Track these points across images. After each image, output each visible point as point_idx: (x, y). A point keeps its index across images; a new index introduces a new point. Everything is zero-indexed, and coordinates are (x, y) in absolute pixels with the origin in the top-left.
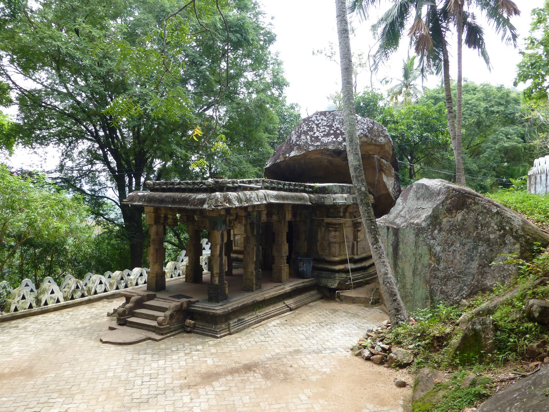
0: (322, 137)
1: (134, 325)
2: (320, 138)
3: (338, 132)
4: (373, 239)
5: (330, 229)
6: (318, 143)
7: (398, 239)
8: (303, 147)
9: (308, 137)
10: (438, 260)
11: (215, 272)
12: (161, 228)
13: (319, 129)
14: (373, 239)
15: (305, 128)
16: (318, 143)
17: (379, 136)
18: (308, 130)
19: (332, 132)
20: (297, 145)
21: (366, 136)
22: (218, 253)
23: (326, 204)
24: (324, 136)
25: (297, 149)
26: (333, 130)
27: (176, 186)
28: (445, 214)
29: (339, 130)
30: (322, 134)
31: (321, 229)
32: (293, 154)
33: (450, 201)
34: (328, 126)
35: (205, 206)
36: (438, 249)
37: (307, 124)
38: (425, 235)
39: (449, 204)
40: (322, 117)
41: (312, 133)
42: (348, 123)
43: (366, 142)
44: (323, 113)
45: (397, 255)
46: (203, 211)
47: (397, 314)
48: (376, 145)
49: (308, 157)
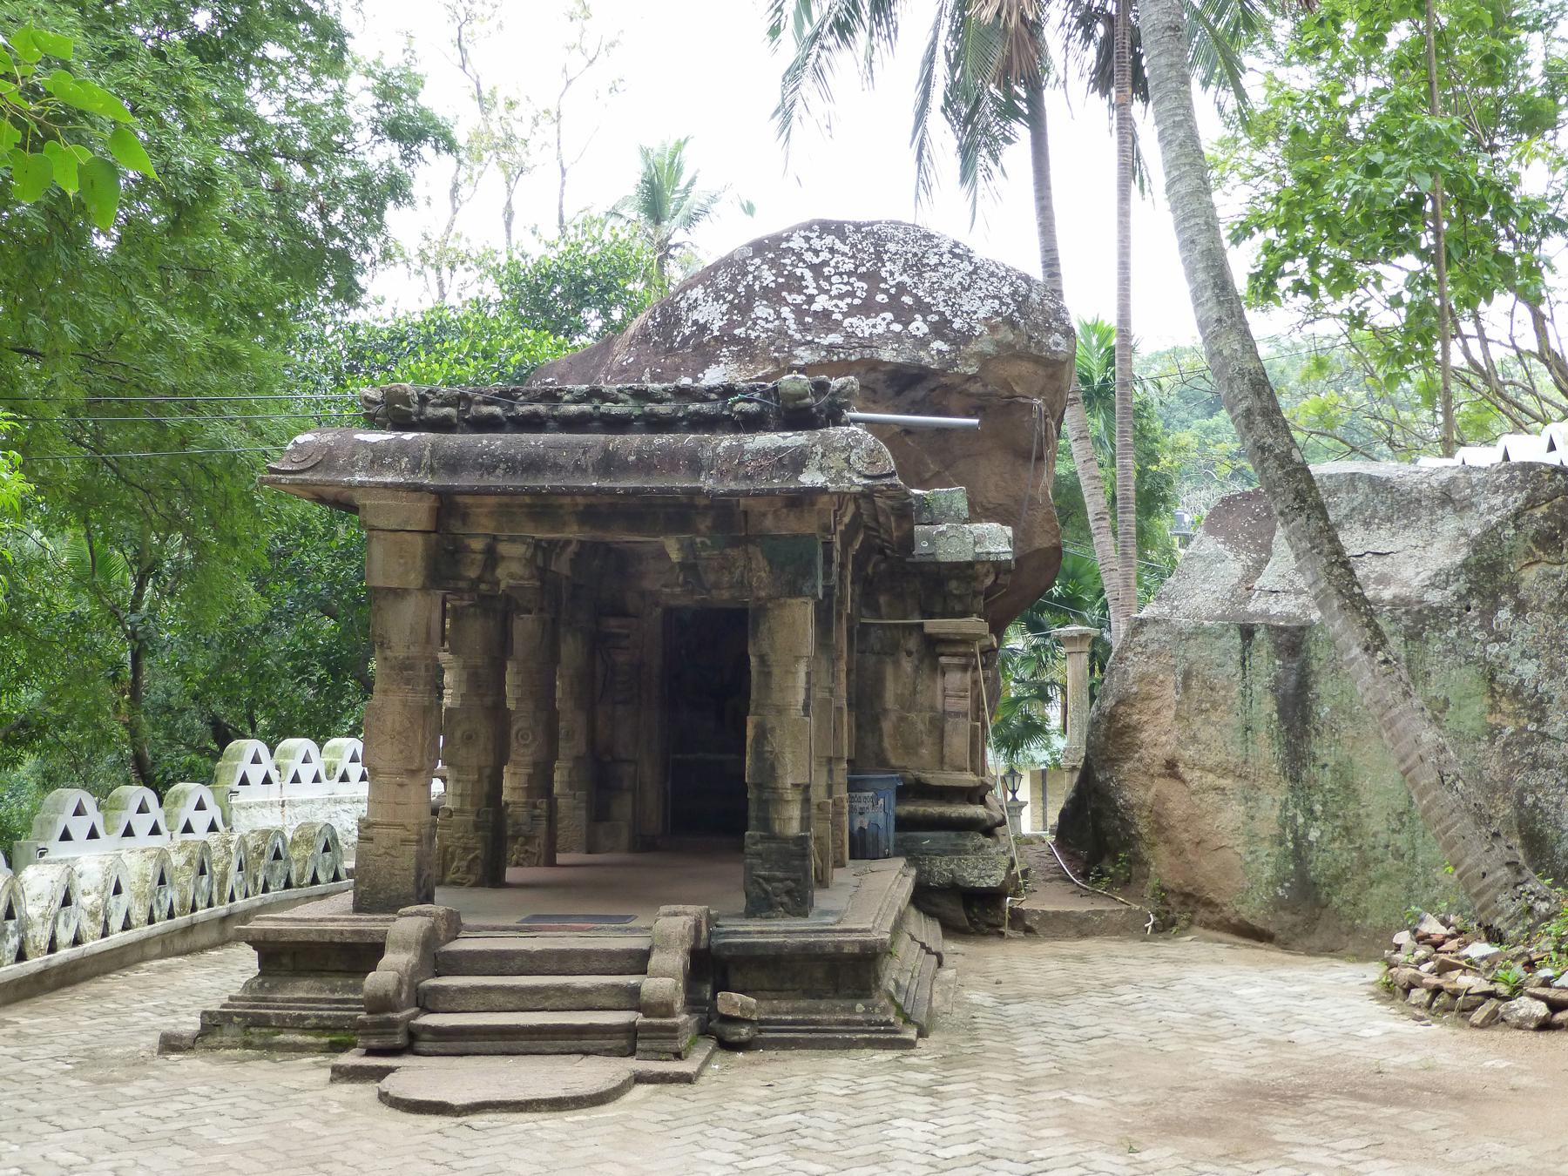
0: (845, 315)
1: (473, 1045)
4: (1368, 632)
5: (943, 660)
6: (835, 338)
7: (1305, 665)
8: (765, 350)
9: (786, 312)
10: (1538, 707)
11: (789, 781)
14: (1368, 632)
15: (768, 277)
16: (835, 338)
17: (1049, 329)
18: (780, 287)
19: (881, 298)
20: (735, 340)
22: (801, 697)
23: (942, 558)
24: (852, 311)
25: (737, 357)
26: (886, 291)
27: (573, 408)
28: (1529, 553)
31: (897, 664)
32: (713, 376)
33: (1544, 508)
34: (861, 277)
35: (811, 478)
36: (1529, 669)
37: (773, 264)
38: (1452, 633)
39: (1545, 518)
40: (829, 240)
41: (799, 299)
42: (1201, 221)
43: (1010, 346)
44: (836, 229)
45: (1305, 720)
46: (802, 499)
47: (1519, 879)
48: (1037, 360)
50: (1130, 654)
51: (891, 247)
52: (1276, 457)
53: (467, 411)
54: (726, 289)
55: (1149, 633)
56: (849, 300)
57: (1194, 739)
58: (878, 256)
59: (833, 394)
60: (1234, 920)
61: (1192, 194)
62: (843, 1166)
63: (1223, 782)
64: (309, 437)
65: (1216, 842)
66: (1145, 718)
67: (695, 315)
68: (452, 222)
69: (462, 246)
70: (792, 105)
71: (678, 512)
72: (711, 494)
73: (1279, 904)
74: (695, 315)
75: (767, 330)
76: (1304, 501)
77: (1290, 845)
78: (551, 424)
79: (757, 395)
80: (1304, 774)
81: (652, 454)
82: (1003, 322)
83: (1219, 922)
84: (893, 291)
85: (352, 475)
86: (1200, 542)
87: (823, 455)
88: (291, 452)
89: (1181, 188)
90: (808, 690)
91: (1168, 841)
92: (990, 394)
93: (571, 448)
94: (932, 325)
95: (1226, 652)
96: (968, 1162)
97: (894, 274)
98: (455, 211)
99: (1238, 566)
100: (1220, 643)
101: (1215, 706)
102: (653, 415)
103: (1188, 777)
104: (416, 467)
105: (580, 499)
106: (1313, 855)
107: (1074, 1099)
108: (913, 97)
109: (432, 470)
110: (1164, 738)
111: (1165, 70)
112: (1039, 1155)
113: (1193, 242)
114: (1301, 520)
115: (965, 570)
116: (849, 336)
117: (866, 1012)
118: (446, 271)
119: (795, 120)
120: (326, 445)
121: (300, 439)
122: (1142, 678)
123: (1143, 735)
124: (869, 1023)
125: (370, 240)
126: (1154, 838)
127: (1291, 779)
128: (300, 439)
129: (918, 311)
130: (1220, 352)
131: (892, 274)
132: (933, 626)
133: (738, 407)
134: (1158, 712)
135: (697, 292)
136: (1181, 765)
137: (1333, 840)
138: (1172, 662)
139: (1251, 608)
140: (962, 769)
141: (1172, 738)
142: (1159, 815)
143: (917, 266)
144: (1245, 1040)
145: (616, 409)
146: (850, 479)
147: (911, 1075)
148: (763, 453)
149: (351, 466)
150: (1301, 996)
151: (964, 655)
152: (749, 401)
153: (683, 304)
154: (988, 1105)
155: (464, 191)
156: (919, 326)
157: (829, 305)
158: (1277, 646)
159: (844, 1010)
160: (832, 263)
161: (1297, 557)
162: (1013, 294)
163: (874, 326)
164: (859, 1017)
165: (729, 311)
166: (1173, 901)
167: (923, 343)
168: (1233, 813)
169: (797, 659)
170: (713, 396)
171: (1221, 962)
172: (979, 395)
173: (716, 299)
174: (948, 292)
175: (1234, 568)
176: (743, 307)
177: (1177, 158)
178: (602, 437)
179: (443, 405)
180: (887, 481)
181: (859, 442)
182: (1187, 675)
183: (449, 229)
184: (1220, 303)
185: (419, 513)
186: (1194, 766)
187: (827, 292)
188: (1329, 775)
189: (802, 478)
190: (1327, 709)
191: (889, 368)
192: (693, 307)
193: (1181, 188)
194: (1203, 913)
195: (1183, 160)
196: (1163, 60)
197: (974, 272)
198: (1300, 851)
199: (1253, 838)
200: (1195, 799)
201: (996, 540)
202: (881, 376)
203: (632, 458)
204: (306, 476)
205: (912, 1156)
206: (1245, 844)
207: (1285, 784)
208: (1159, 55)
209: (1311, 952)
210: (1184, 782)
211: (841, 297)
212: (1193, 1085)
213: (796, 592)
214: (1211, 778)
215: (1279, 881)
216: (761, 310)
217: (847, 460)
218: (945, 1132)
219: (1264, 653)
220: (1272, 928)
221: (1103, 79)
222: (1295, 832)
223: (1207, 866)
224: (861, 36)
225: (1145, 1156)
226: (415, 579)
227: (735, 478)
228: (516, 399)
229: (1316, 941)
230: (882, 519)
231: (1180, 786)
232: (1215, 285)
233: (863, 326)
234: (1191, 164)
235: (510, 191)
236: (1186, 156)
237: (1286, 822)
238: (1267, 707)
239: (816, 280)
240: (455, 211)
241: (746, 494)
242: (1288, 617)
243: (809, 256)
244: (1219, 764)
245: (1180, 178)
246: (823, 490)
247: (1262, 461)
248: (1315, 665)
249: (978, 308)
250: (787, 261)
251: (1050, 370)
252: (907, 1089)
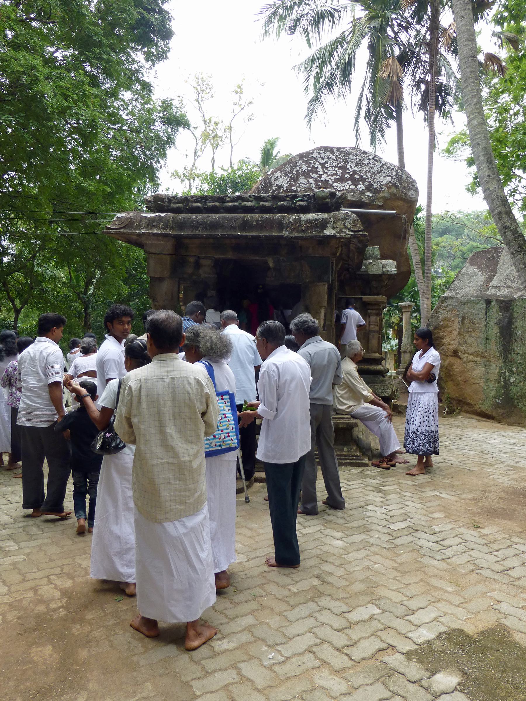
0: (334, 182)
2: (330, 182)
5: (369, 311)
7: (511, 315)
9: (311, 180)
13: (326, 171)
15: (305, 168)
17: (409, 189)
19: (347, 176)
21: (395, 185)
23: (371, 272)
24: (336, 180)
26: (349, 173)
29: (358, 174)
30: (333, 178)
34: (340, 168)
35: (329, 232)
37: (307, 163)
40: (327, 154)
42: (482, 135)
44: (330, 150)
45: (511, 336)
50: (440, 310)
52: (511, 231)
53: (188, 205)
54: (289, 172)
55: (449, 302)
57: (465, 342)
59: (337, 198)
60: (478, 411)
61: (479, 125)
62: (349, 533)
63: (476, 359)
64: (123, 215)
65: (472, 381)
66: (445, 334)
67: (277, 183)
68: (194, 164)
69: (198, 172)
70: (312, 114)
71: (275, 246)
72: (288, 238)
73: (497, 405)
74: (277, 183)
75: (304, 188)
76: (522, 248)
77: (503, 383)
78: (222, 210)
79: (306, 198)
80: (509, 357)
81: (263, 221)
83: (472, 411)
84: (351, 173)
85: (140, 230)
86: (467, 268)
87: (334, 222)
88: (115, 220)
89: (474, 122)
90: (325, 320)
91: (452, 380)
93: (229, 219)
94: (366, 186)
95: (479, 310)
96: (406, 533)
97: (351, 167)
98: (195, 160)
99: (483, 277)
100: (477, 306)
101: (474, 330)
102: (263, 206)
103: (462, 356)
104: (166, 227)
105: (233, 241)
106: (512, 388)
107: (443, 495)
108: (354, 112)
109: (172, 228)
111: (469, 74)
112: (437, 529)
113: (478, 144)
114: (521, 256)
115: (379, 277)
117: (348, 451)
118: (192, 180)
119: (312, 120)
120: (130, 218)
121: (119, 215)
122: (445, 319)
123: (444, 341)
124: (349, 456)
125: (160, 160)
126: (447, 379)
128: (119, 215)
129: (361, 181)
130: (489, 189)
131: (351, 167)
132: (366, 298)
133: (298, 203)
134: (451, 332)
135: (278, 174)
136: (459, 352)
137: (521, 382)
138: (458, 313)
139: (489, 293)
140: (375, 352)
141: (456, 342)
142: (450, 371)
143: (360, 164)
144: (502, 465)
145: (248, 204)
146: (345, 232)
147: (369, 480)
148: (309, 221)
149: (139, 227)
150: (515, 444)
151: (377, 309)
152: (303, 201)
153: (273, 178)
154: (406, 498)
155: (199, 153)
156: (361, 187)
157: (328, 178)
158: (500, 307)
159: (339, 450)
161: (518, 271)
162: (397, 174)
164: (345, 453)
165: (290, 181)
166: (454, 403)
167: (362, 193)
168: (480, 371)
169: (321, 307)
170: (288, 199)
171: (476, 427)
173: (285, 176)
174: (372, 174)
175: (481, 278)
176: (295, 179)
177: (473, 110)
178: (242, 215)
179: (178, 203)
180: (361, 233)
181: (349, 217)
182: (463, 318)
183: (193, 166)
184: (489, 169)
185: (168, 246)
186: (465, 352)
187: (327, 173)
188: (519, 357)
189: (325, 232)
190: (520, 332)
192: (276, 180)
193: (474, 122)
194: (466, 408)
195: (475, 111)
196: (468, 70)
197: (382, 166)
198: (507, 386)
199: (487, 380)
200: (465, 365)
201: (390, 266)
203: (254, 223)
204: (122, 231)
205: (379, 528)
206: (484, 382)
207: (501, 360)
208: (467, 68)
209: (510, 424)
210: (460, 358)
211: (332, 175)
212: (491, 489)
213: (320, 279)
214: (471, 357)
215: (497, 397)
216: (302, 180)
217: (344, 224)
218: (391, 514)
219: (495, 310)
220: (494, 414)
221: (423, 106)
222: (505, 379)
223: (468, 390)
224: (336, 89)
225: (485, 531)
226: (166, 274)
227: (297, 232)
228: (207, 200)
229: (512, 420)
230: (351, 255)
231: (459, 360)
232: (487, 162)
233: (340, 186)
234: (478, 113)
235: (214, 153)
236: (477, 109)
238: (495, 331)
239: (323, 169)
240: (195, 160)
241: (302, 238)
242: (505, 296)
243: (320, 160)
244: (475, 352)
245: (474, 118)
246: (334, 236)
247: (505, 233)
248: (516, 315)
249: (383, 180)
250: (312, 162)
252: (369, 488)
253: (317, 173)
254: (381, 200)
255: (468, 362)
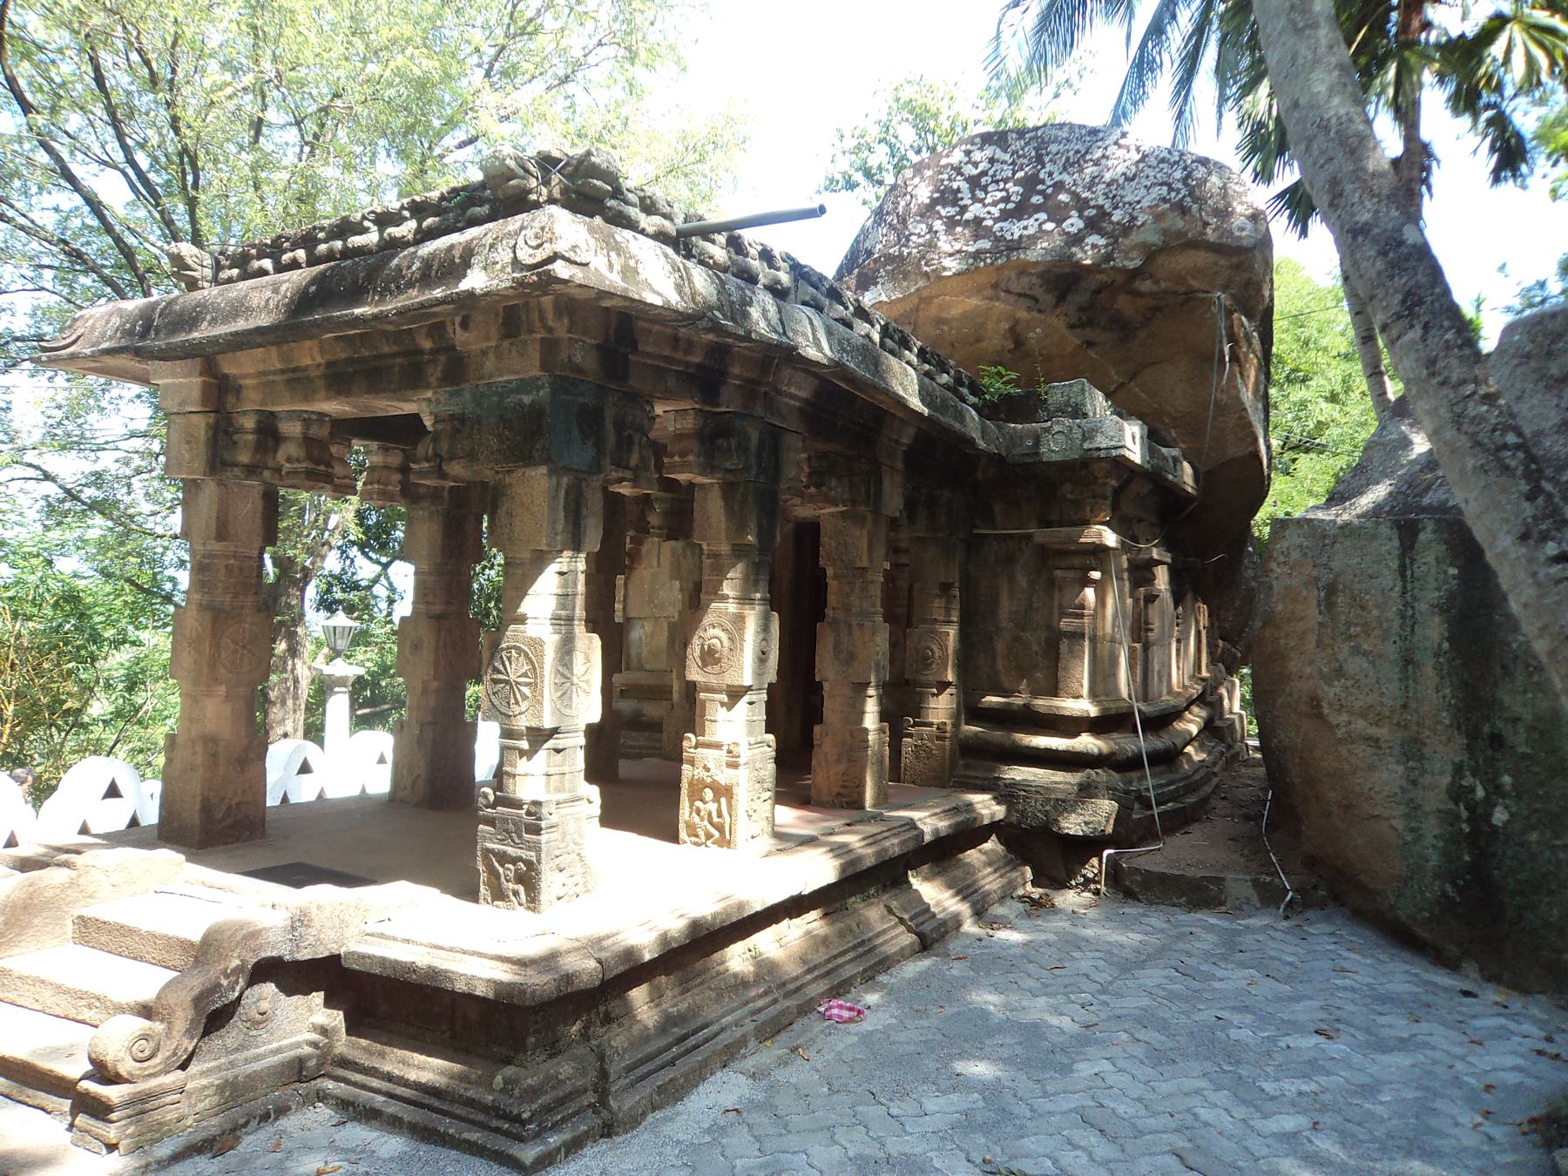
0: (996, 220)
2: (989, 223)
3: (1063, 197)
5: (1058, 573)
12: (248, 507)
24: (1005, 216)
25: (892, 276)
26: (1042, 193)
30: (995, 211)
31: (1012, 579)
35: (475, 280)
41: (951, 211)
43: (1180, 234)
48: (1217, 248)
49: (933, 311)
51: (1053, 148)
56: (1002, 206)
57: (1340, 673)
58: (1039, 159)
63: (1374, 731)
77: (1466, 828)
82: (1171, 209)
84: (1049, 191)
92: (1165, 292)
103: (1334, 720)
110: (1308, 670)
116: (998, 239)
127: (1468, 736)
156: (1074, 223)
160: (991, 172)
162: (1185, 180)
163: (1025, 228)
172: (1151, 294)
182: (1331, 590)
187: (981, 201)
191: (1040, 269)
199: (1413, 807)
202: (1035, 280)
211: (994, 204)
214: (1360, 725)
219: (1431, 559)
237: (1458, 793)
238: (1433, 631)
251: (1235, 260)
253: (955, 203)
254: (1134, 254)
255: (1350, 739)
